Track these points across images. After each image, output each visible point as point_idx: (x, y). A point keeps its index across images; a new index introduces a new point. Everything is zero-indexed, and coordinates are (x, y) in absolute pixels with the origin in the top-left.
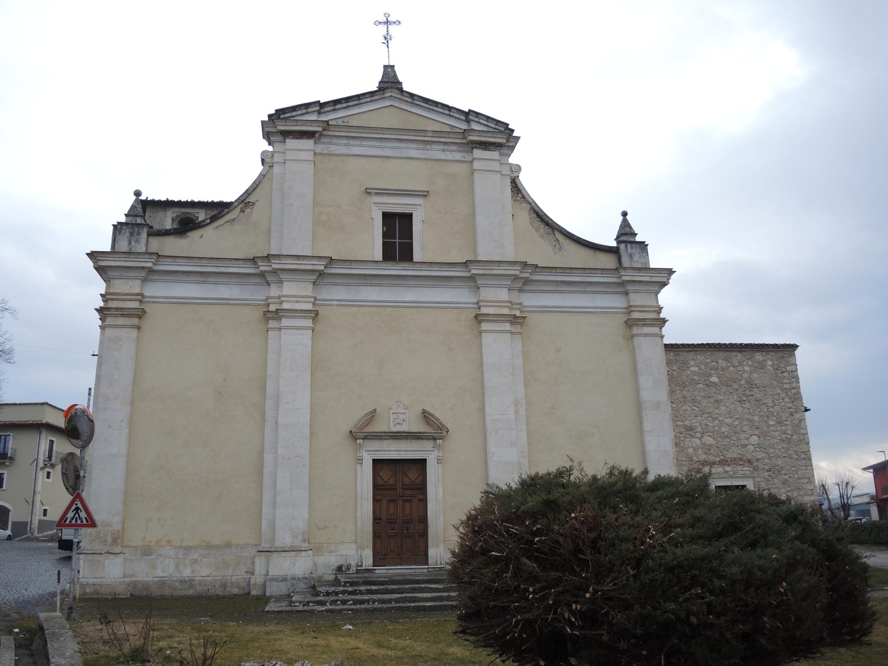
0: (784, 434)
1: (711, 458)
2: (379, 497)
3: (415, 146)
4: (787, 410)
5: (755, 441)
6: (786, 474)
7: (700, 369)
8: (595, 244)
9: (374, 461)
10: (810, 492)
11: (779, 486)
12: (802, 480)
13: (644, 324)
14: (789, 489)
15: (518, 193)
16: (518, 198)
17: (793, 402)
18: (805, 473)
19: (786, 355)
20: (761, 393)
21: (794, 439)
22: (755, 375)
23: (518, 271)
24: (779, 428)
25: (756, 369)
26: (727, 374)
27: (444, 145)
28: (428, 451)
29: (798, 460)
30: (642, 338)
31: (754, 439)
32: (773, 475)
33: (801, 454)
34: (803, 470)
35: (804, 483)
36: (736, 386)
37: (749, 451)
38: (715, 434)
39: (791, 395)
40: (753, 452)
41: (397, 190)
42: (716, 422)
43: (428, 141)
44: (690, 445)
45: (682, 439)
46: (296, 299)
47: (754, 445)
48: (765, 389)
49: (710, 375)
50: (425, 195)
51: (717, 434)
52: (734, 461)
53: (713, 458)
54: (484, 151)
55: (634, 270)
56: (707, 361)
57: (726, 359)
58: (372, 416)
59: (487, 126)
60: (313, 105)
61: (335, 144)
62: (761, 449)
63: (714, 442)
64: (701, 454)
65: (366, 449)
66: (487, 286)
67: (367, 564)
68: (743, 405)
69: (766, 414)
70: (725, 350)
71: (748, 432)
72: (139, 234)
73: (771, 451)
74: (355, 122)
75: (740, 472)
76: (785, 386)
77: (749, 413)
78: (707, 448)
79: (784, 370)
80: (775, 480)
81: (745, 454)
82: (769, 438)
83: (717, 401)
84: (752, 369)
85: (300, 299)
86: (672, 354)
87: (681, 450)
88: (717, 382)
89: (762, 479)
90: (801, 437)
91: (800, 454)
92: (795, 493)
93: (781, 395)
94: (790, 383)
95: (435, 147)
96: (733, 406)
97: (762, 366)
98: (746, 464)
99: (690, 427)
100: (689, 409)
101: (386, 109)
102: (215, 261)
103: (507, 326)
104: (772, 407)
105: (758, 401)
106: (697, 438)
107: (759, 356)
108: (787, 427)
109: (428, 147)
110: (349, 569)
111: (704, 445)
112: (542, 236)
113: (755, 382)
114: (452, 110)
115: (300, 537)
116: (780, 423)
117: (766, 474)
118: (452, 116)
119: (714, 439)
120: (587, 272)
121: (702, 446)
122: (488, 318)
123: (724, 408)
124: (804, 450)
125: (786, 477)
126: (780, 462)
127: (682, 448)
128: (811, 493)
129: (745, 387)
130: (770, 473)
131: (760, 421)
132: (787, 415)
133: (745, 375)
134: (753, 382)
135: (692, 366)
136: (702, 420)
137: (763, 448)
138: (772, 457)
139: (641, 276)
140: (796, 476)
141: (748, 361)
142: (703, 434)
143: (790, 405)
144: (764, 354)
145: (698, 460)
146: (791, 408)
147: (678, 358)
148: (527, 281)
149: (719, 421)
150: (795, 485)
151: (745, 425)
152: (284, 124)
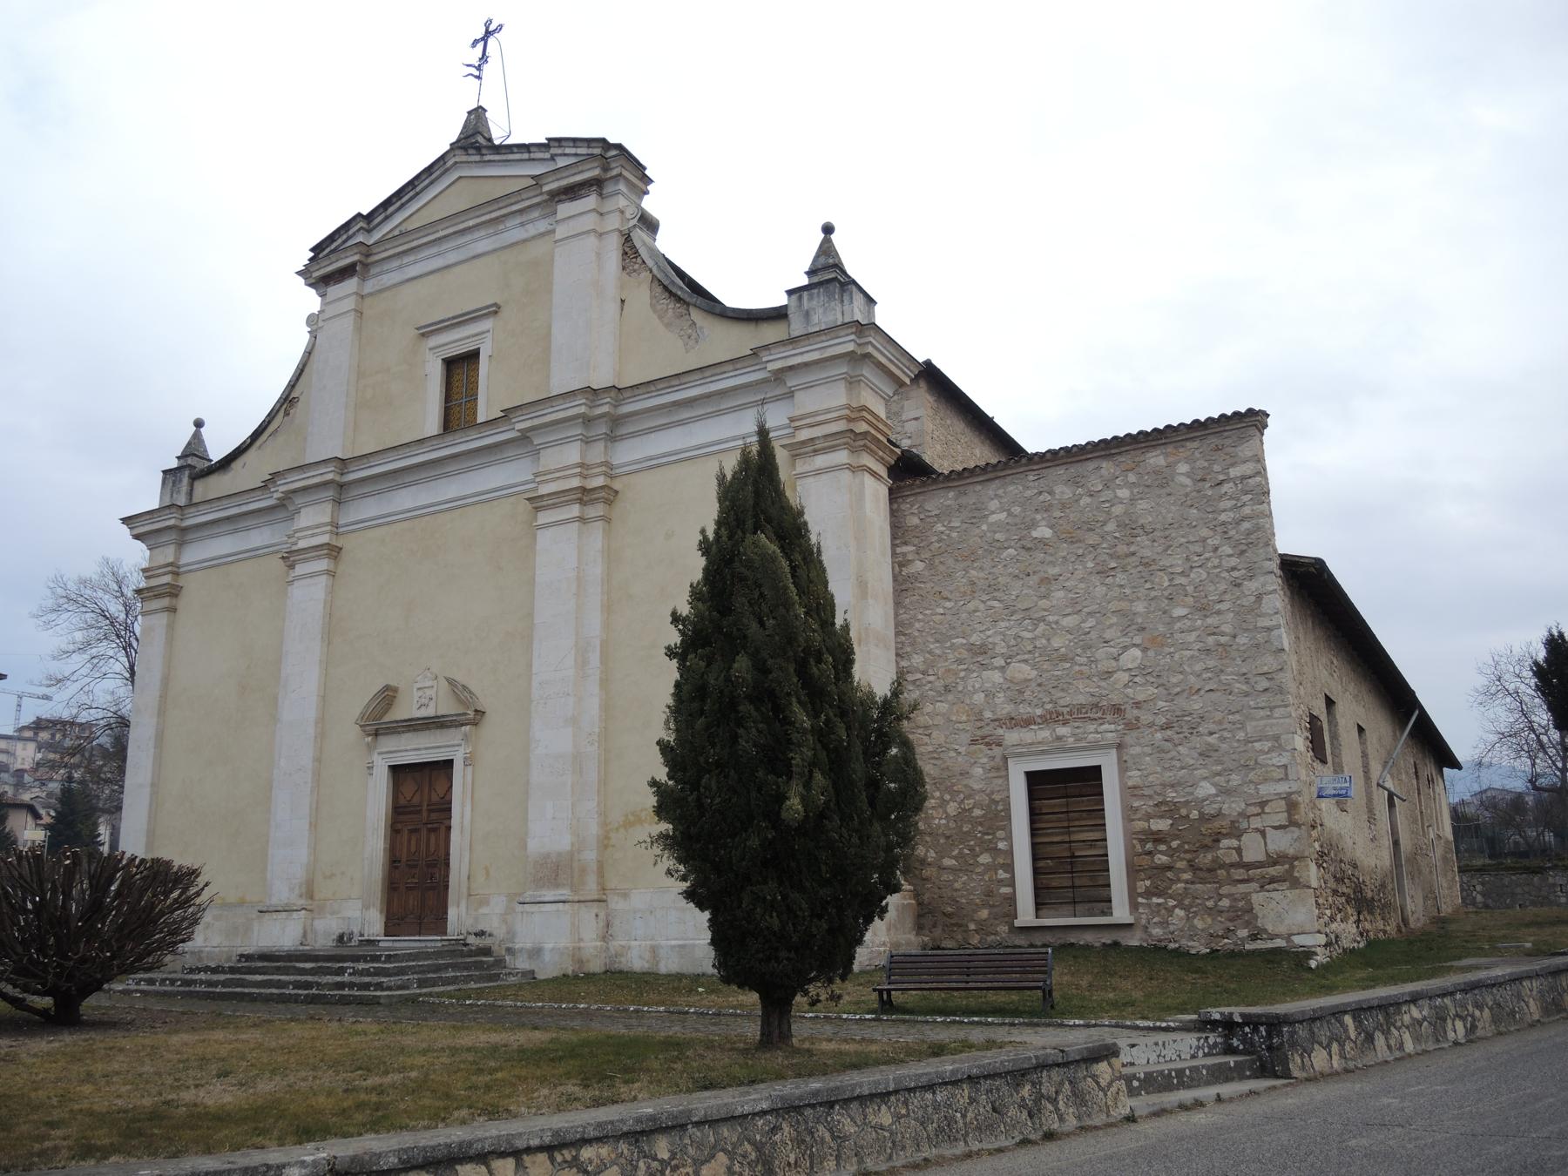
0: (1214, 634)
1: (1024, 710)
2: (399, 826)
3: (483, 233)
4: (1225, 574)
5: (1133, 661)
6: (1211, 734)
7: (1010, 514)
8: (751, 310)
9: (395, 769)
10: (1279, 774)
11: (1192, 762)
12: (1255, 744)
13: (815, 451)
14: (1219, 768)
15: (636, 257)
16: (636, 267)
17: (1243, 552)
18: (1265, 726)
19: (1228, 442)
20: (1156, 544)
21: (1238, 644)
22: (1143, 505)
23: (583, 407)
24: (1199, 622)
25: (1146, 490)
26: (1071, 515)
27: (521, 214)
28: (453, 746)
29: (1247, 694)
30: (811, 480)
31: (1134, 656)
32: (1176, 736)
33: (1258, 678)
34: (1262, 718)
35: (1262, 752)
36: (1092, 539)
37: (1117, 686)
38: (1037, 655)
39: (1237, 537)
40: (1126, 686)
41: (454, 318)
42: (1042, 626)
43: (497, 218)
44: (977, 686)
45: (962, 674)
46: (310, 532)
47: (1130, 669)
48: (1167, 533)
49: (1034, 525)
50: (494, 311)
51: (1041, 655)
52: (1080, 713)
53: (1029, 709)
54: (575, 203)
55: (784, 345)
56: (1028, 493)
57: (1075, 482)
58: (388, 696)
59: (576, 155)
60: (354, 223)
61: (387, 272)
62: (1148, 678)
63: (1035, 673)
64: (1003, 703)
65: (379, 751)
66: (548, 445)
67: (371, 932)
68: (1109, 580)
69: (1166, 593)
70: (1069, 460)
71: (1118, 641)
72: (181, 481)
73: (1174, 680)
74: (410, 226)
75: (1092, 735)
76: (1223, 517)
77: (1124, 597)
78: (1017, 691)
79: (1221, 477)
80: (1180, 748)
81: (1104, 692)
82: (1172, 650)
83: (1045, 581)
84: (1136, 490)
85: (315, 531)
86: (951, 494)
87: (959, 698)
88: (1047, 536)
89: (1148, 750)
90: (1260, 637)
91: (1252, 681)
92: (1233, 776)
93: (1209, 541)
94: (1235, 507)
95: (510, 223)
96: (1082, 585)
97: (1163, 479)
98: (1109, 717)
99: (982, 645)
100: (982, 607)
101: (453, 188)
102: (233, 500)
103: (575, 510)
104: (1182, 574)
105: (1147, 565)
106: (996, 668)
107: (1156, 459)
108: (1221, 617)
109: (501, 227)
110: (350, 940)
111: (1011, 682)
112: (668, 325)
113: (1141, 521)
114: (532, 149)
115: (297, 891)
116: (1203, 609)
117: (1159, 735)
118: (534, 160)
119: (1034, 667)
120: (708, 373)
121: (1005, 686)
122: (545, 503)
123: (1061, 594)
124: (1266, 669)
125: (1211, 740)
126: (1196, 705)
127: (960, 695)
128: (1282, 776)
129: (1116, 538)
130: (1169, 732)
131: (1149, 613)
132: (1222, 587)
133: (1118, 510)
134: (1136, 522)
135: (993, 513)
136: (1008, 628)
137: (1154, 674)
138: (1177, 694)
139: (802, 353)
140: (1241, 735)
141: (1127, 476)
142: (1008, 659)
143: (1234, 561)
144: (1170, 449)
145: (995, 717)
146: (1234, 569)
147: (963, 500)
148: (616, 421)
149: (1049, 624)
150: (1233, 757)
151: (1111, 626)
152: (318, 267)
